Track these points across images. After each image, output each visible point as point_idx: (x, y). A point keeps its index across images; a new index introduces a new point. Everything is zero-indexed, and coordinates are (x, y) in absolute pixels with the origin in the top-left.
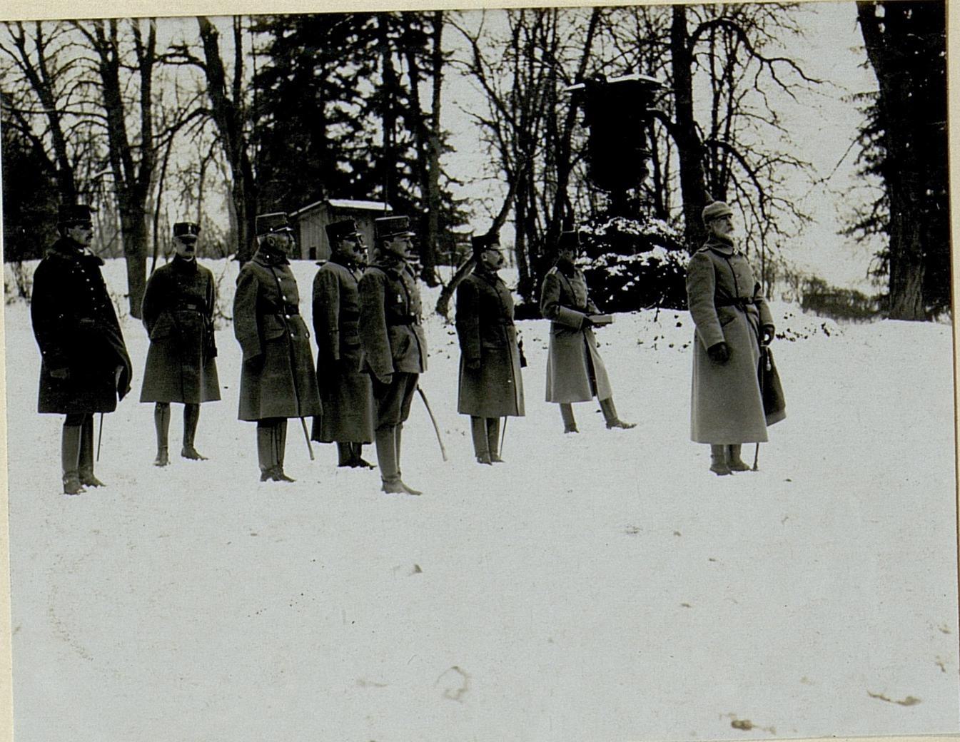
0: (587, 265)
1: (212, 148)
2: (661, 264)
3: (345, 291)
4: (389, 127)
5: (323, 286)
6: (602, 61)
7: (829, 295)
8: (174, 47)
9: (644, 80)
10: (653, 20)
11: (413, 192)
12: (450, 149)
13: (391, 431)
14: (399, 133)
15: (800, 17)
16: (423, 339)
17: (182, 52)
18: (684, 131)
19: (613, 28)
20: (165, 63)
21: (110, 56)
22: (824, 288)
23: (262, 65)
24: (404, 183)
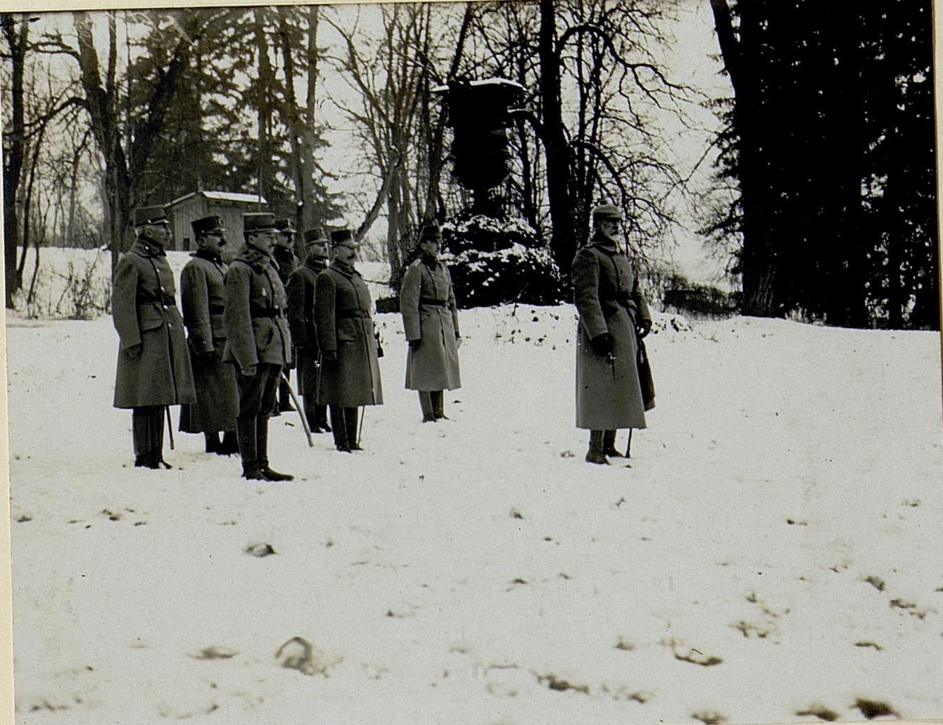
0: (449, 260)
1: (85, 137)
2: (520, 261)
3: (212, 287)
4: (264, 117)
5: (190, 280)
6: (474, 62)
7: (690, 292)
8: (47, 36)
10: (523, 23)
11: (288, 185)
12: (325, 143)
14: (275, 127)
15: (664, 25)
17: (55, 41)
18: (551, 129)
19: (486, 29)
20: (38, 51)
24: (280, 177)
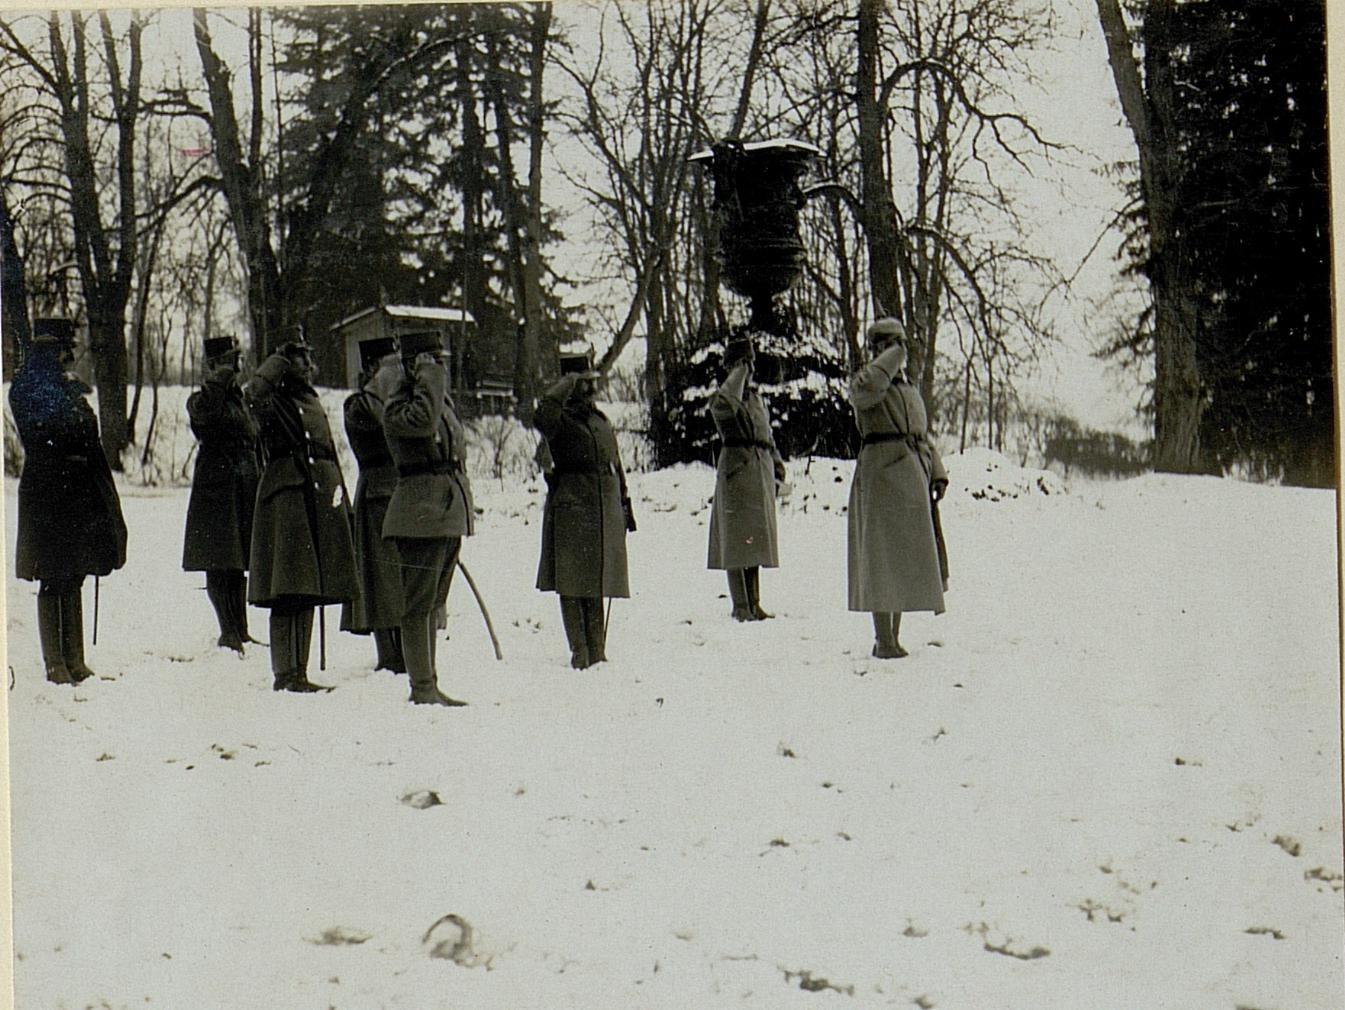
2: (817, 397)
4: (471, 203)
6: (766, 117)
8: (166, 91)
9: (793, 147)
12: (558, 236)
13: (424, 622)
16: (470, 494)
21: (75, 102)
22: (1074, 431)
23: (290, 117)
24: (495, 284)
